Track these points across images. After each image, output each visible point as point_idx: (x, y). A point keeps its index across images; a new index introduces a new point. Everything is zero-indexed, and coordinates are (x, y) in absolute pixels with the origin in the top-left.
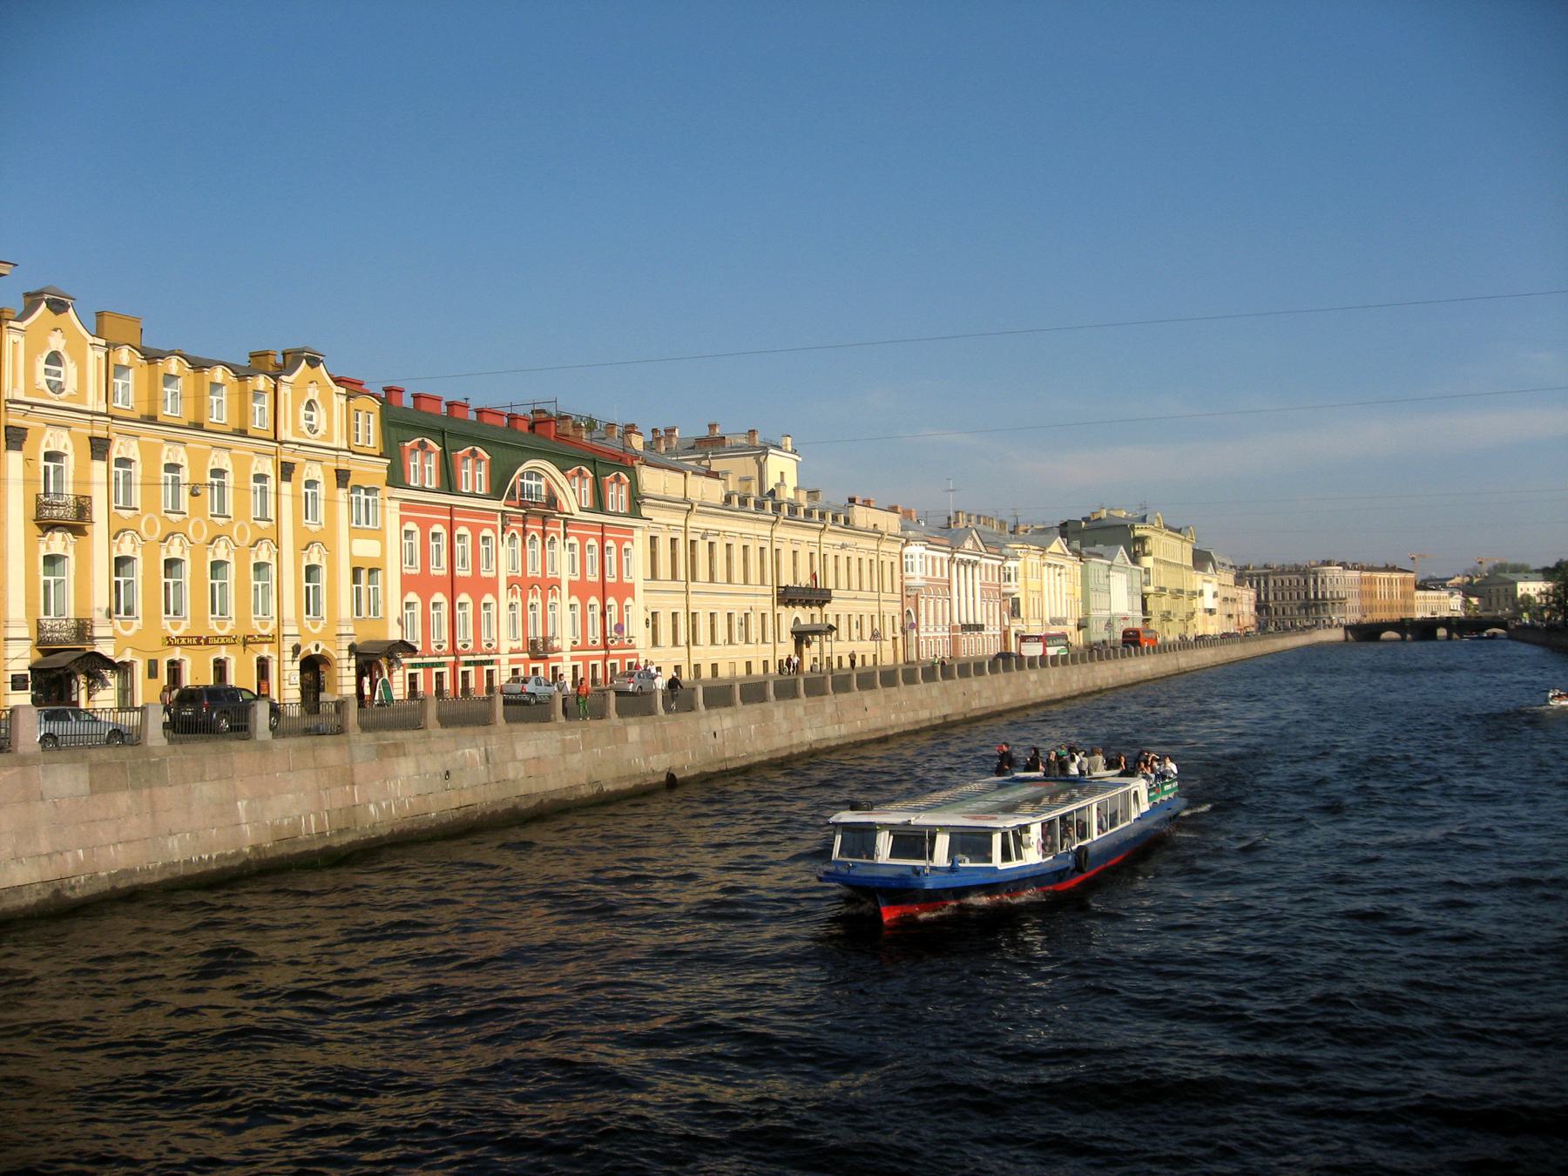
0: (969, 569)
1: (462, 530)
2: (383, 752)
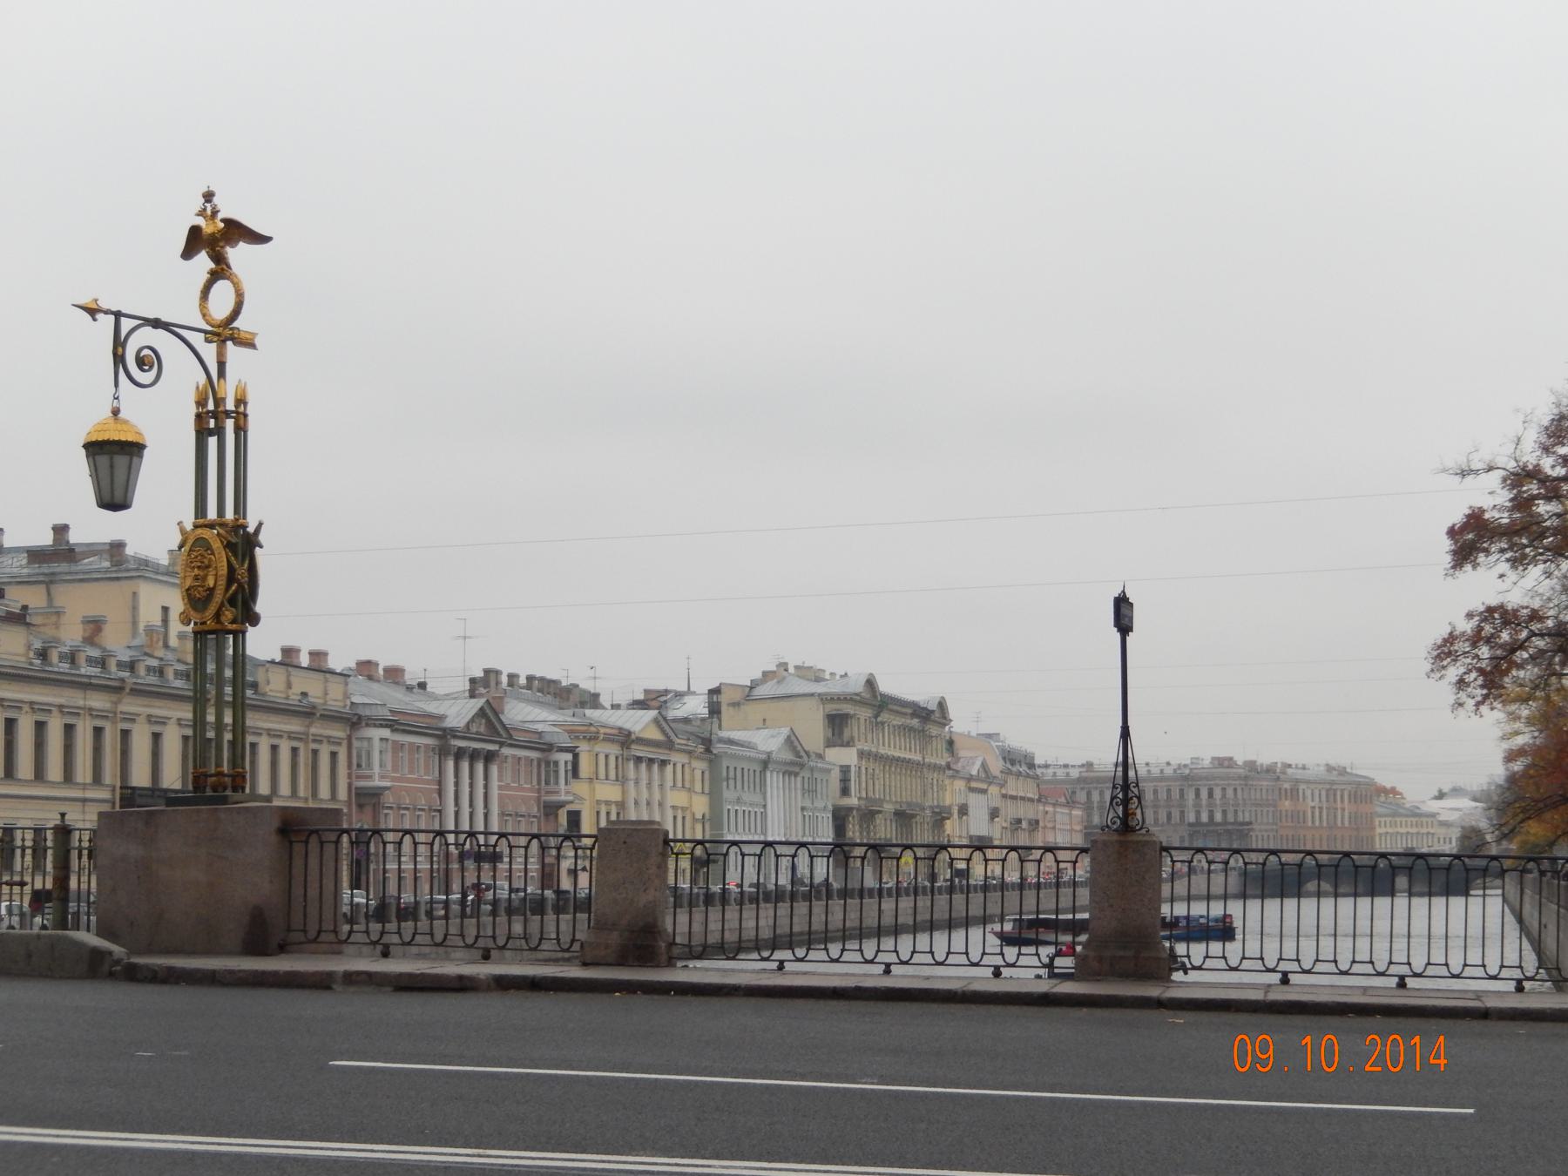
0: (480, 767)
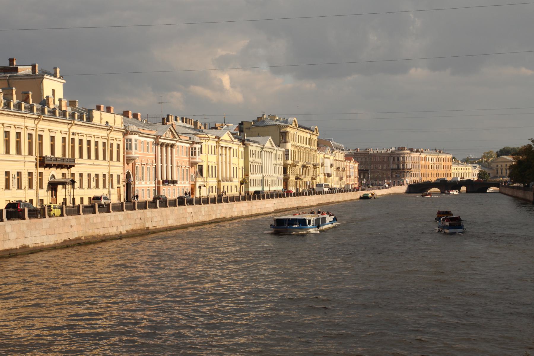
0: (169, 149)
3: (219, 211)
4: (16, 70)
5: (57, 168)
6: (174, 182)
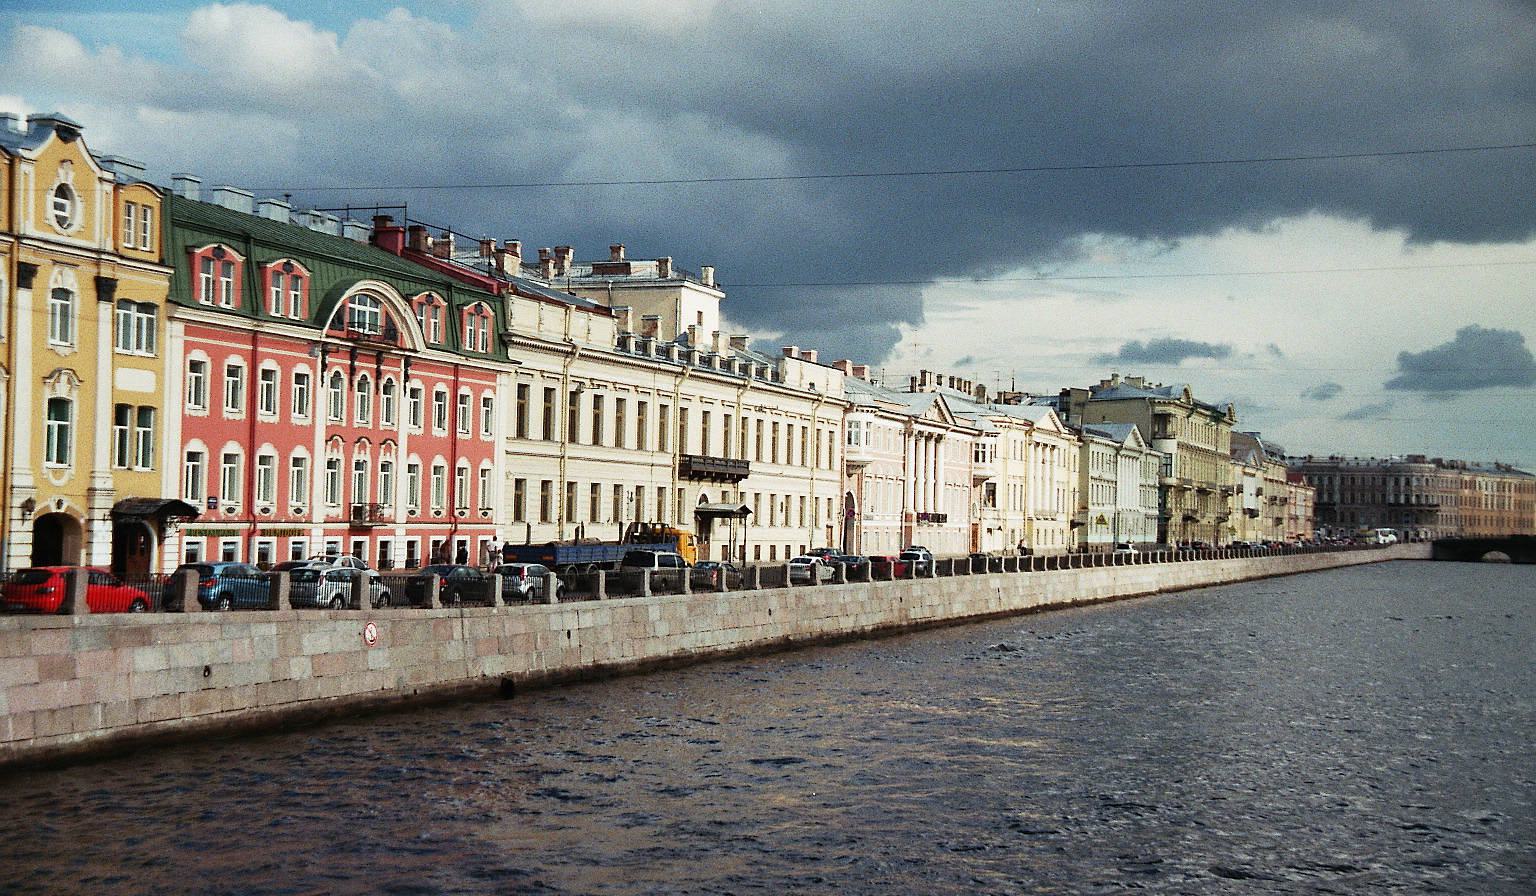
0: (932, 444)
1: (268, 364)
2: (112, 639)
3: (1050, 588)
4: (626, 268)
5: (713, 480)
6: (940, 519)
